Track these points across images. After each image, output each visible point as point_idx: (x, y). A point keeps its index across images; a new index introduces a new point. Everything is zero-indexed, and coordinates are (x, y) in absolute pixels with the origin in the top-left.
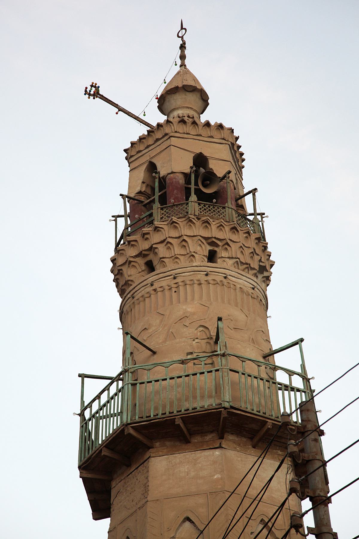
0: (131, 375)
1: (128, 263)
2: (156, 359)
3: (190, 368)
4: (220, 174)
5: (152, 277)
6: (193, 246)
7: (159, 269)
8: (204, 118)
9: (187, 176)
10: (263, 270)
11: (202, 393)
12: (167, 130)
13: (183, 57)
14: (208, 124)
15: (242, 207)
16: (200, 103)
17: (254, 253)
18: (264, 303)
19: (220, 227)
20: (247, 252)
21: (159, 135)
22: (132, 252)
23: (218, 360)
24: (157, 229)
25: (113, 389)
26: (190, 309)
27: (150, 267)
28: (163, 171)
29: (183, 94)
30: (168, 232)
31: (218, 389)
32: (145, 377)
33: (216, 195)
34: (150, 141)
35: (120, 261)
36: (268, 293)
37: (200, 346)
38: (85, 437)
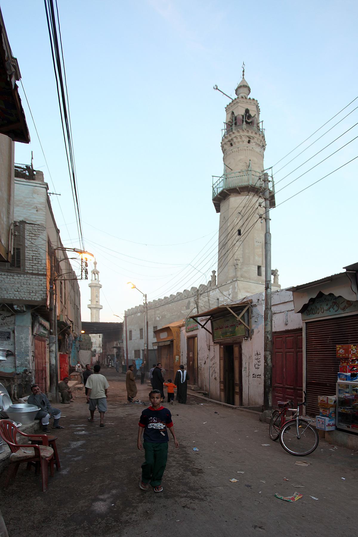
0: (226, 176)
1: (225, 144)
2: (232, 172)
3: (241, 174)
4: (252, 115)
5: (232, 148)
6: (244, 138)
7: (234, 145)
8: (249, 97)
9: (243, 116)
10: (263, 147)
11: (244, 181)
12: (238, 100)
13: (243, 75)
14: (250, 98)
15: (259, 127)
16: (248, 92)
17: (261, 141)
18: (263, 156)
19: (252, 132)
20: (259, 140)
21: (235, 102)
22: (226, 140)
23: (249, 172)
24: (233, 133)
25: (221, 180)
26: (242, 157)
27: (231, 145)
28: (236, 114)
29: (243, 88)
30: (237, 134)
31: (248, 180)
32: (229, 176)
33: (251, 122)
34: (233, 104)
35: (223, 143)
36: (264, 154)
37: (245, 168)
38: (214, 193)
